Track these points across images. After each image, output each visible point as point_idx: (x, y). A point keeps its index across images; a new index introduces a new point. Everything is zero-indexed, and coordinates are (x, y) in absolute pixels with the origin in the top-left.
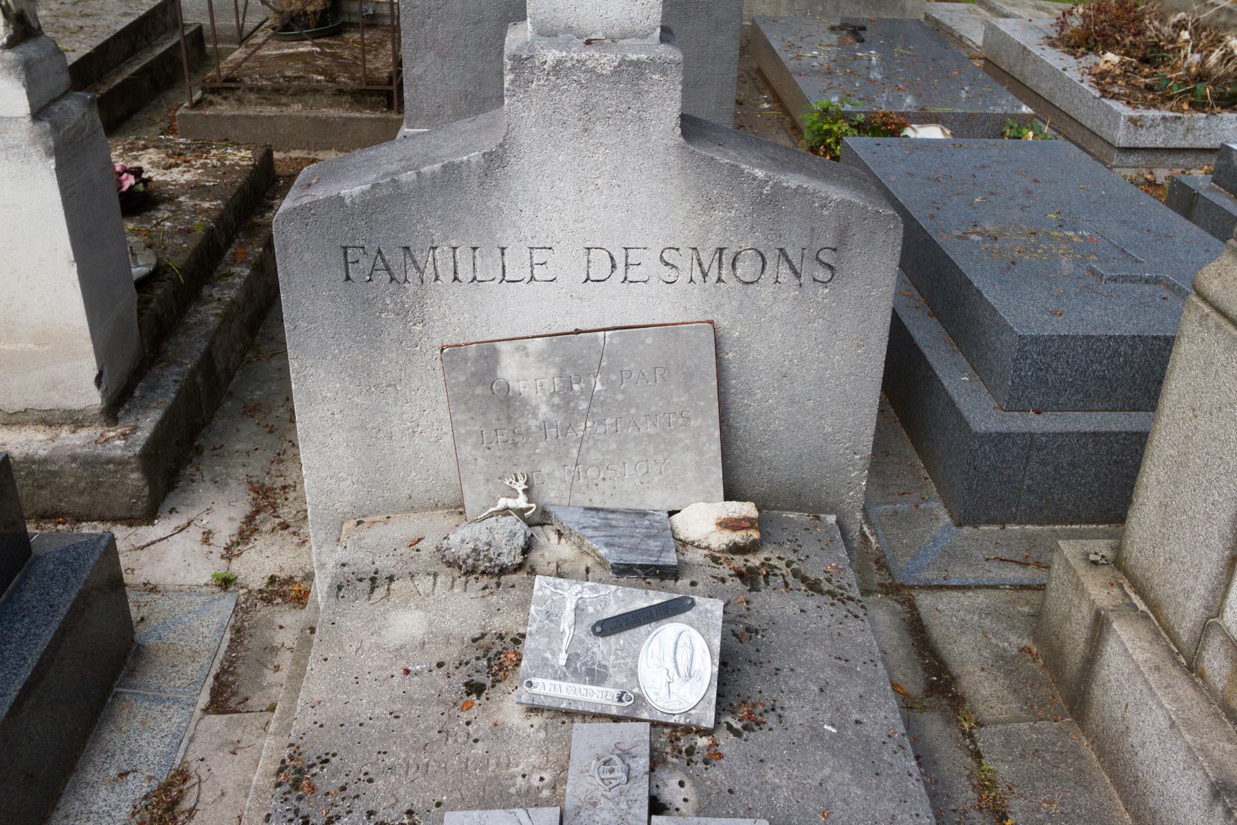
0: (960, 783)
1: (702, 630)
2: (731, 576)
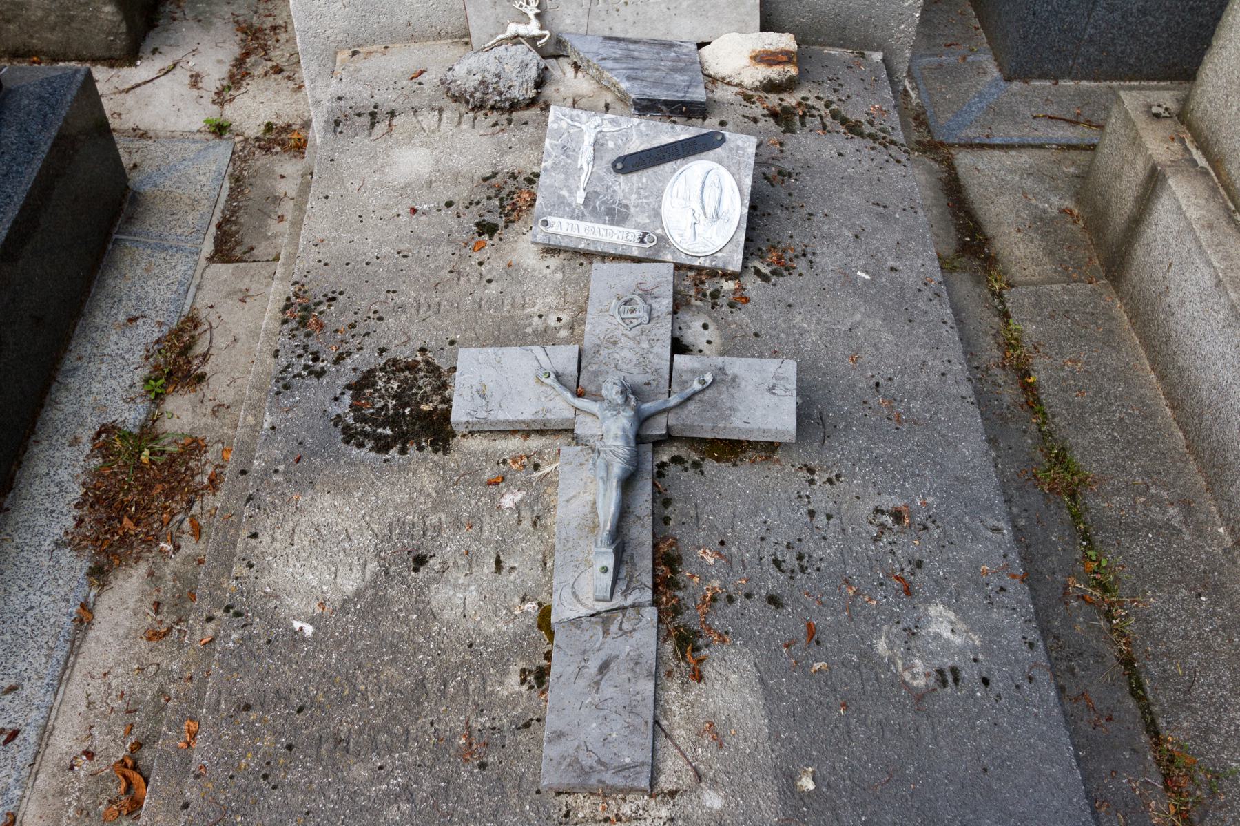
0: (985, 342)
1: (733, 169)
2: (764, 115)
